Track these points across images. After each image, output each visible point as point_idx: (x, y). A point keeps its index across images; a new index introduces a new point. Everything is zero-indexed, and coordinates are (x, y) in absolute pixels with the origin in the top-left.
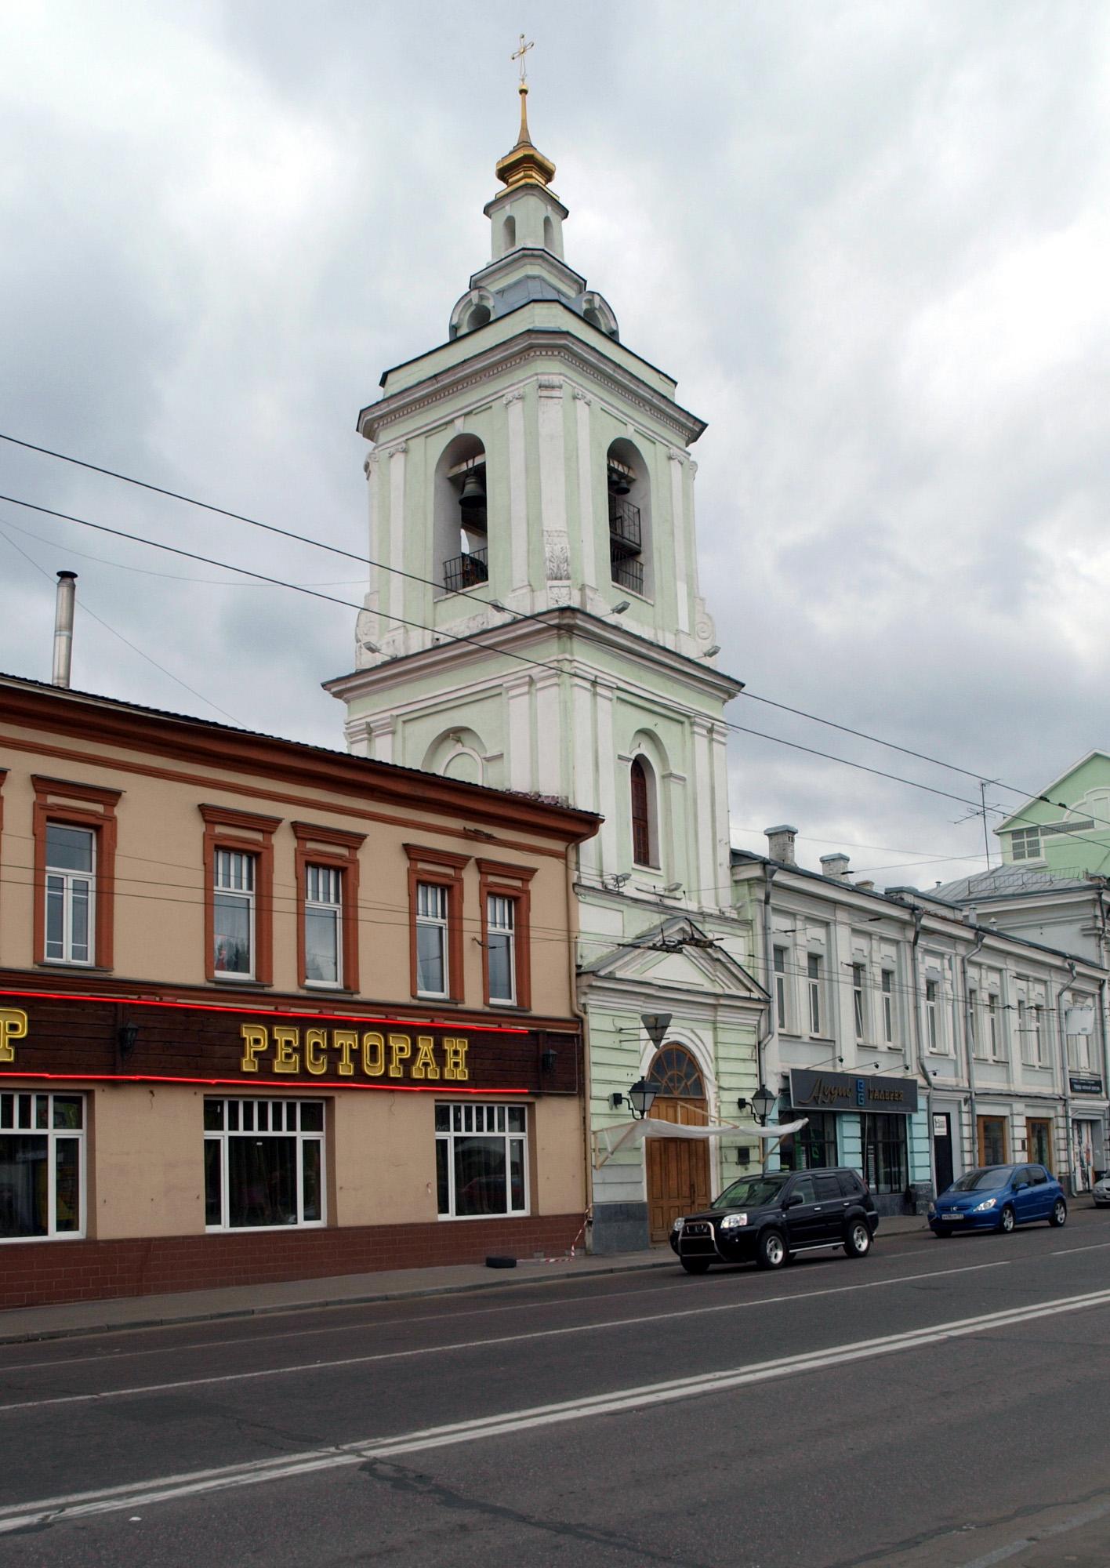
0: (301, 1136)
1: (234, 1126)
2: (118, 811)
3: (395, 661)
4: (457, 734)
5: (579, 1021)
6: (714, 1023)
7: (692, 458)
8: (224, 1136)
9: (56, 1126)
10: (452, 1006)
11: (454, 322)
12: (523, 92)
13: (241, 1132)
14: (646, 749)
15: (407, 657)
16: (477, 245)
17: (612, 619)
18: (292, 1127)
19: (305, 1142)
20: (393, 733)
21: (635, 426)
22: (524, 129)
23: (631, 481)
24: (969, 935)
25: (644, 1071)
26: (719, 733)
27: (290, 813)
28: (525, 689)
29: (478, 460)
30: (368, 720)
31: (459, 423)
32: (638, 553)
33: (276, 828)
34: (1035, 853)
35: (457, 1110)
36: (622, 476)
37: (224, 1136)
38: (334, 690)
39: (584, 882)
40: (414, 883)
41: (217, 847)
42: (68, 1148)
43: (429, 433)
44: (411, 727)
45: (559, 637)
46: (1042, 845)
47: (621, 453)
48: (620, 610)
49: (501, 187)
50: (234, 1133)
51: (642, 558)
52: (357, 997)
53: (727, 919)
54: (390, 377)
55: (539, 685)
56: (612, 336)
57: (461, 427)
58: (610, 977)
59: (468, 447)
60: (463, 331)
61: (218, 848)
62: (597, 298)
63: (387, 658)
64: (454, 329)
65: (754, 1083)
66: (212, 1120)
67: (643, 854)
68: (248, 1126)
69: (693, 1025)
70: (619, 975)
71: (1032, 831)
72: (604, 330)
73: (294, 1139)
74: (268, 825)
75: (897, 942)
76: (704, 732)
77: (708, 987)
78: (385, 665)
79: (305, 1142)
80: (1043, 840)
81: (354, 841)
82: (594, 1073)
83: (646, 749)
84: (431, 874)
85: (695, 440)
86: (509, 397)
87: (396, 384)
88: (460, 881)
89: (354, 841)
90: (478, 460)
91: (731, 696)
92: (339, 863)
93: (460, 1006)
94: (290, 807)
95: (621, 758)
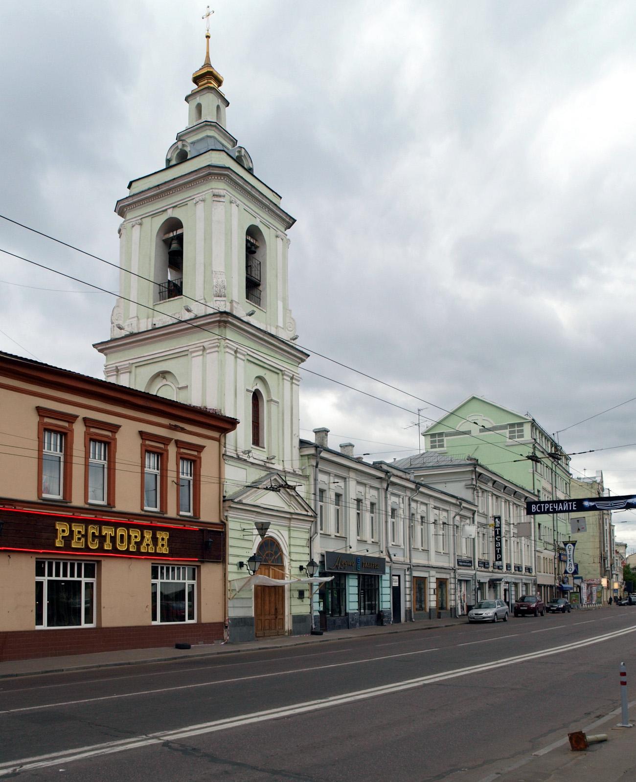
0: (84, 580)
1: (50, 575)
2: (117, 436)
3: (132, 335)
4: (164, 374)
5: (223, 524)
6: (289, 527)
7: (288, 237)
8: (45, 579)
9: (85, 577)
10: (161, 515)
11: (168, 158)
12: (208, 37)
13: (54, 578)
14: (260, 387)
15: (139, 333)
16: (181, 118)
17: (246, 319)
18: (79, 575)
19: (86, 583)
20: (130, 372)
21: (261, 219)
22: (208, 57)
23: (257, 247)
24: (413, 486)
25: (254, 551)
26: (296, 379)
27: (82, 413)
28: (201, 353)
29: (179, 232)
30: (117, 365)
31: (170, 211)
32: (259, 285)
33: (118, 430)
34: (442, 446)
35: (162, 568)
36: (252, 244)
37: (45, 579)
38: (99, 348)
39: (228, 454)
40: (179, 457)
41: (45, 429)
42: (89, 586)
43: (153, 215)
44: (139, 369)
45: (219, 327)
46: (445, 440)
47: (253, 233)
48: (250, 315)
49: (195, 86)
50: (162, 581)
51: (261, 288)
52: (114, 509)
53: (297, 474)
54: (134, 185)
55: (208, 351)
56: (250, 171)
57: (170, 213)
58: (240, 503)
59: (174, 225)
60: (173, 162)
61: (45, 430)
62: (243, 151)
63: (128, 333)
64: (168, 161)
65: (307, 558)
66: (40, 572)
67: (257, 440)
68: (58, 575)
69: (278, 528)
70: (244, 501)
71: (441, 434)
72: (246, 167)
73: (81, 581)
74: (71, 419)
75: (378, 489)
76: (289, 379)
77: (287, 509)
78: (127, 337)
79: (86, 583)
80: (445, 439)
81: (115, 428)
82: (231, 551)
83: (260, 387)
84: (153, 446)
85: (289, 228)
86: (197, 199)
87: (137, 188)
88: (167, 451)
89: (115, 428)
90: (179, 232)
91: (303, 361)
92: (193, 458)
93: (165, 515)
94: (83, 410)
95: (248, 390)
